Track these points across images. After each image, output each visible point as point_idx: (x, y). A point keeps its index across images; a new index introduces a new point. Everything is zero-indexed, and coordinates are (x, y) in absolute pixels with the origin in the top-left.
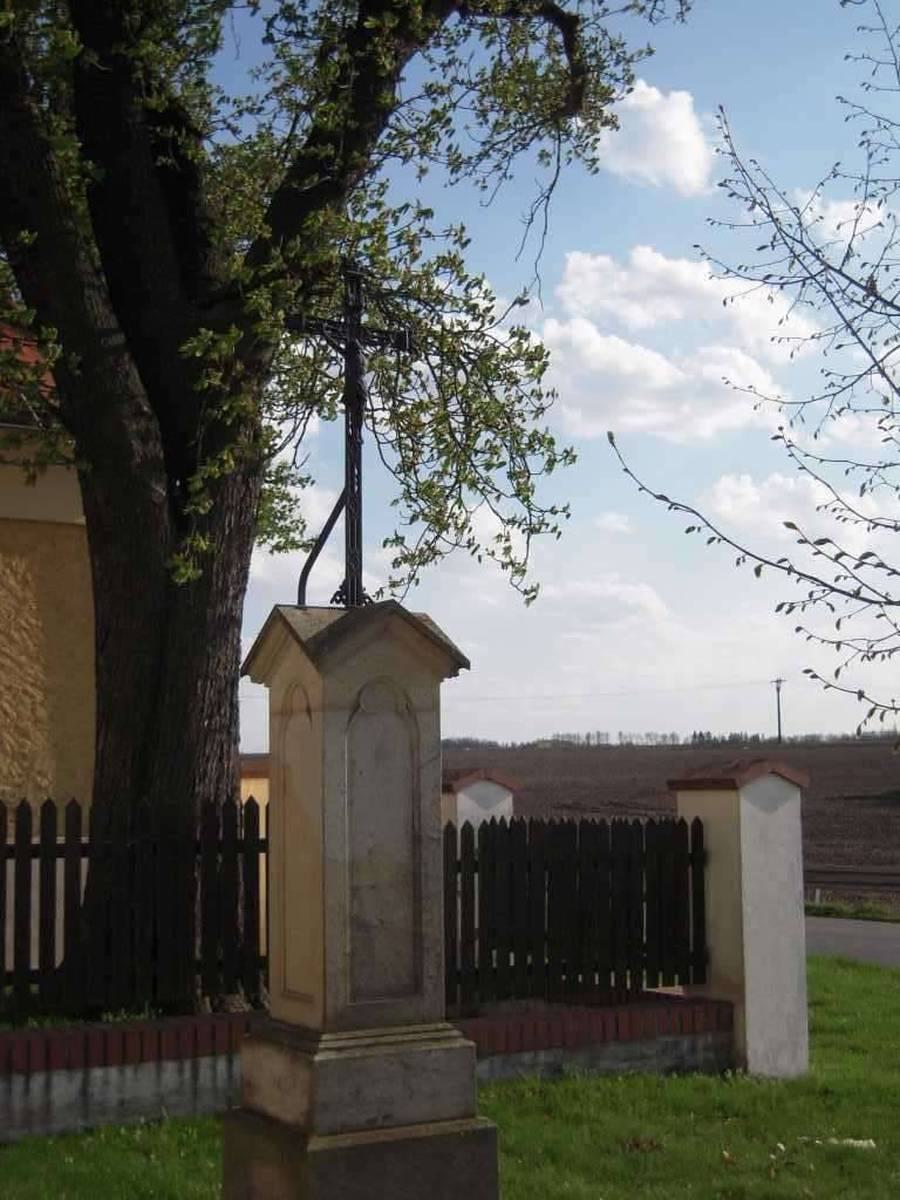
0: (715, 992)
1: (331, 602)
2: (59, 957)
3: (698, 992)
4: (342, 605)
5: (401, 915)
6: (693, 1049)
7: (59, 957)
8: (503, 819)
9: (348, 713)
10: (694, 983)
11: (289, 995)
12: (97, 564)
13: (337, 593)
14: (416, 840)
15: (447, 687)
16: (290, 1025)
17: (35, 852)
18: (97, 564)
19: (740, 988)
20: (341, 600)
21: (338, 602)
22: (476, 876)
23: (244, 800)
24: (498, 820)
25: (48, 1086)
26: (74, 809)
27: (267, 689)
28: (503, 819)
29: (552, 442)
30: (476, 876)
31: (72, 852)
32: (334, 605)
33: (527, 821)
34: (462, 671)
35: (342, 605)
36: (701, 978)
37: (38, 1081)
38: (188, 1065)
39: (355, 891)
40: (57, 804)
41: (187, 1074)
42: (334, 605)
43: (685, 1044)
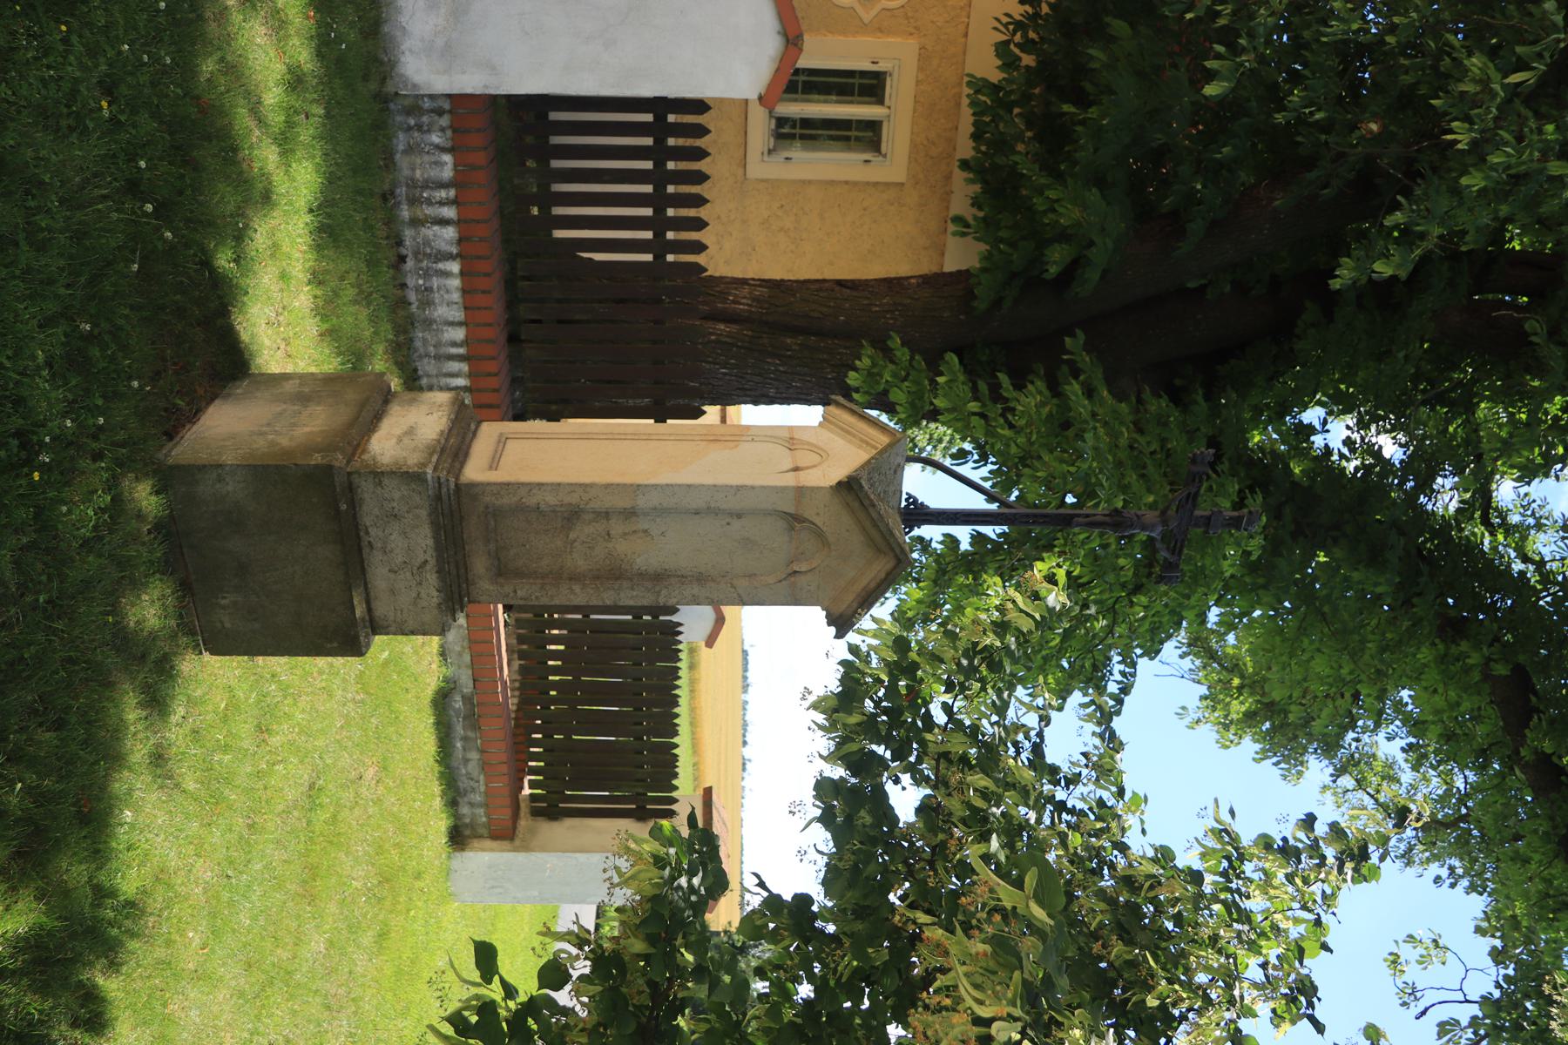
0: (524, 822)
1: (910, 496)
2: (560, 234)
3: (524, 808)
4: (904, 504)
5: (579, 561)
6: (471, 805)
7: (560, 234)
8: (681, 633)
9: (792, 510)
10: (880, 101)
11: (502, 441)
12: (913, 281)
13: (915, 500)
14: (658, 578)
15: (817, 614)
16: (469, 447)
17: (659, 234)
18: (913, 281)
19: (526, 848)
20: (909, 504)
21: (907, 500)
22: (630, 617)
23: (705, 408)
24: (679, 629)
25: (444, 222)
26: (699, 247)
27: (816, 424)
28: (681, 633)
29: (1458, 1022)
30: (630, 617)
31: (659, 247)
32: (904, 496)
33: (679, 664)
34: (833, 630)
35: (904, 504)
36: (536, 813)
37: (449, 212)
38: (461, 351)
39: (606, 515)
40: (703, 255)
41: (454, 351)
42: (904, 496)
43: (478, 798)
